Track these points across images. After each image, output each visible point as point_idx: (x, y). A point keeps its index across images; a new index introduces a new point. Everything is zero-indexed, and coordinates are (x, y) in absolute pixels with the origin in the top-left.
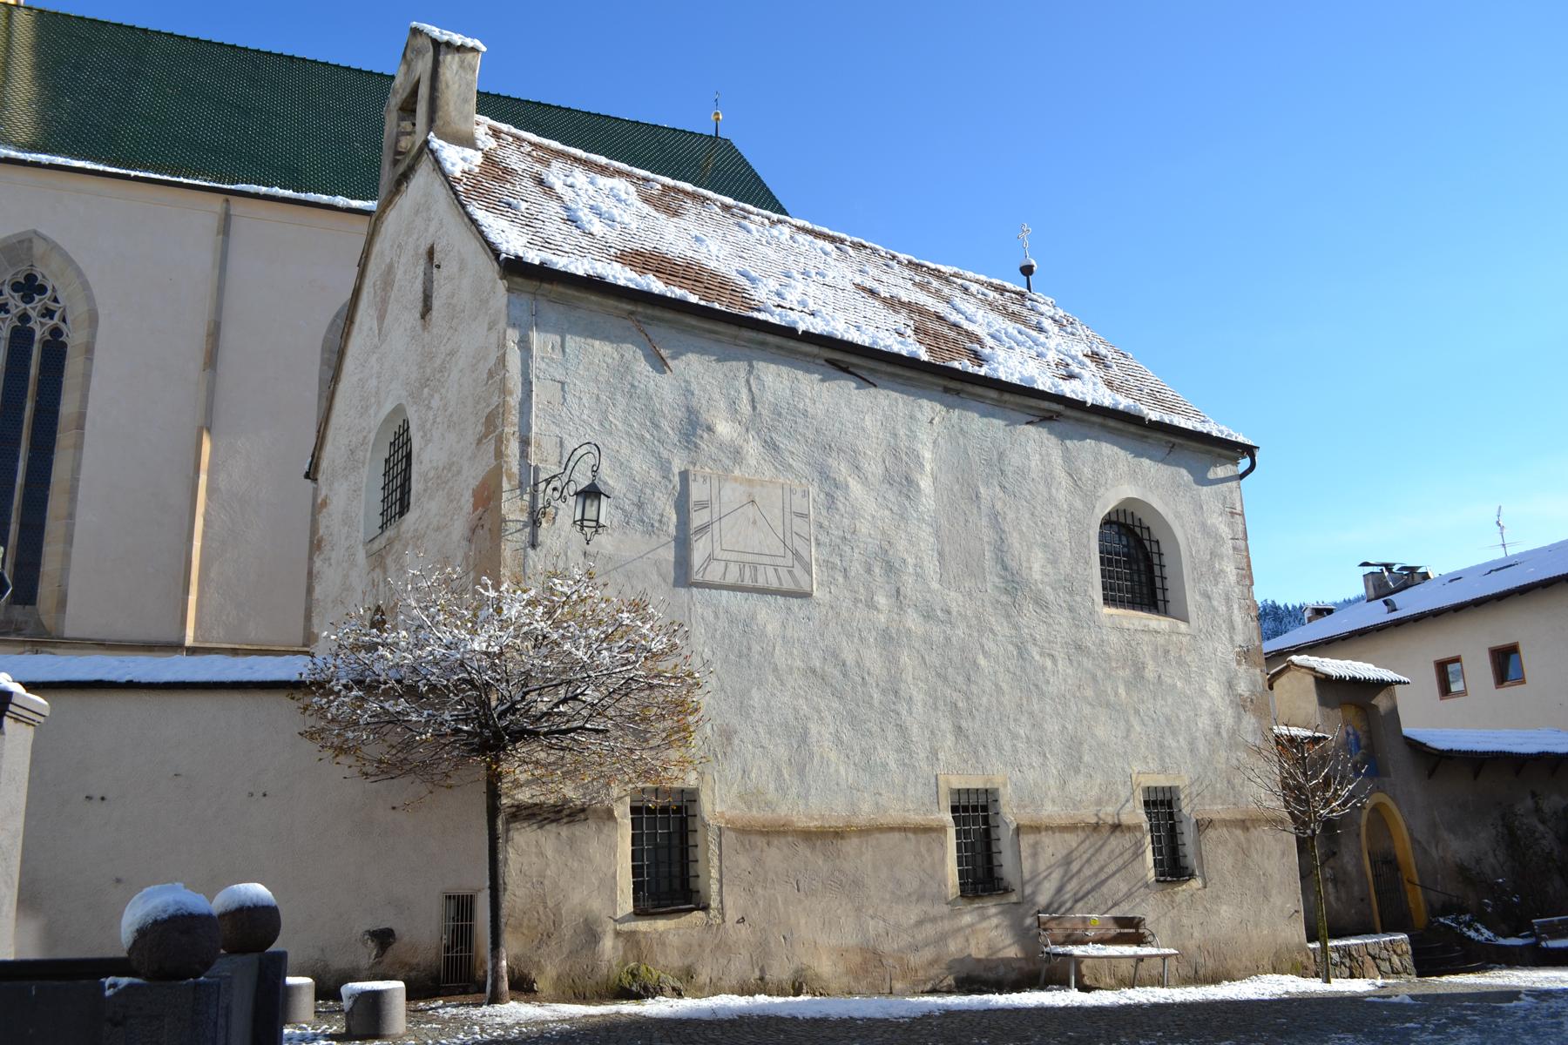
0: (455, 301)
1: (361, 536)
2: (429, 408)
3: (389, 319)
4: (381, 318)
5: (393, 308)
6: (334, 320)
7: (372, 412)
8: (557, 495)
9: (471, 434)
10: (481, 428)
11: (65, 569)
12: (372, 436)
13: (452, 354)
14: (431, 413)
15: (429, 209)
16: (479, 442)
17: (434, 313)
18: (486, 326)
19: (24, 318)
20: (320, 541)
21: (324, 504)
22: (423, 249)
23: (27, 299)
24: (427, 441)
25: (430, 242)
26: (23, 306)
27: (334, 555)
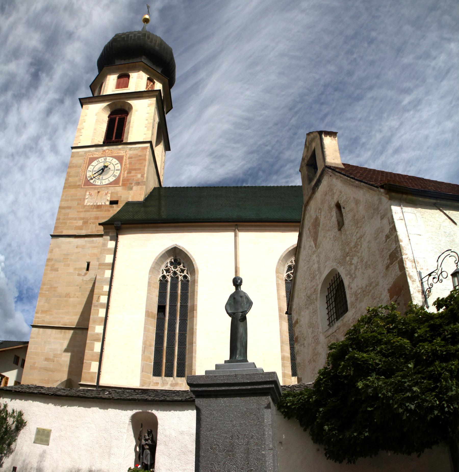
0: (356, 218)
1: (320, 330)
2: (351, 264)
3: (320, 238)
4: (315, 239)
5: (321, 234)
6: (279, 262)
7: (317, 278)
8: (436, 280)
9: (381, 266)
10: (387, 261)
11: (281, 324)
12: (319, 287)
13: (361, 237)
14: (353, 267)
15: (332, 190)
16: (387, 268)
17: (346, 226)
18: (379, 219)
19: (175, 273)
20: (297, 338)
21: (297, 322)
22: (333, 204)
23: (175, 267)
24: (353, 277)
25: (336, 202)
26: (174, 270)
27: (306, 343)
